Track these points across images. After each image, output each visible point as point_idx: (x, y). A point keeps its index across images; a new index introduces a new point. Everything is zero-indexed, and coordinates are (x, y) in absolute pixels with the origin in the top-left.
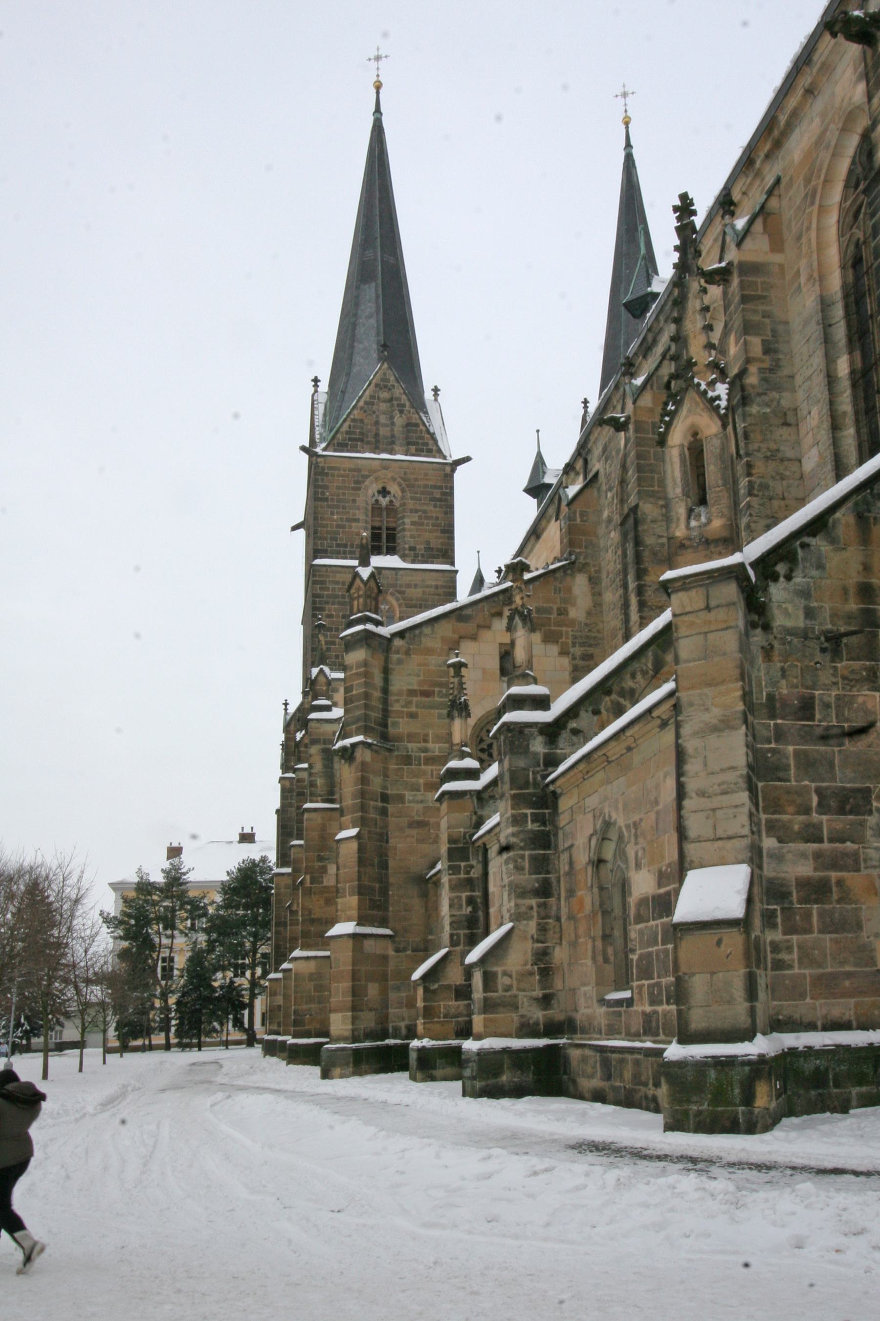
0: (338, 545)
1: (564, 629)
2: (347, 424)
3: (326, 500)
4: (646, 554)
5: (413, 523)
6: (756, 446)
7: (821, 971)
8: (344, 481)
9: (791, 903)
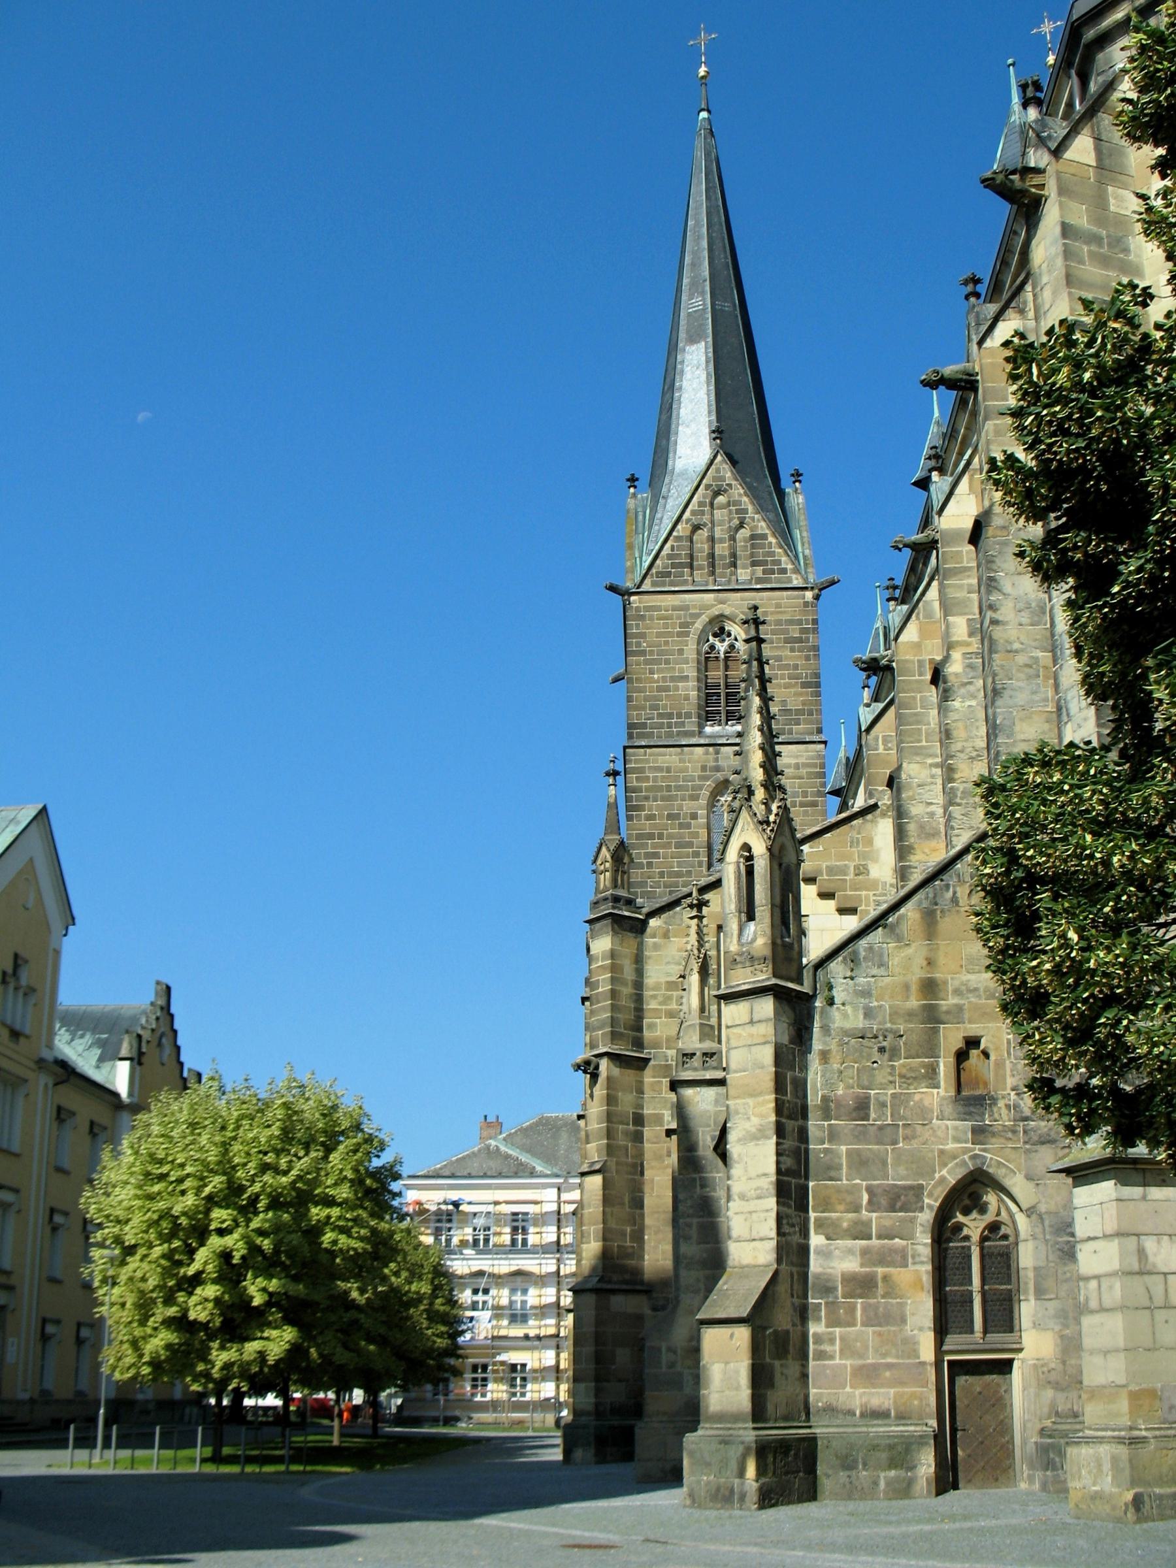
0: (660, 716)
1: (864, 893)
2: (668, 545)
3: (643, 653)
4: (912, 828)
6: (959, 746)
7: (861, 1362)
8: (666, 626)
9: (837, 1298)
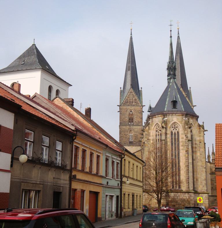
5: (136, 117)
